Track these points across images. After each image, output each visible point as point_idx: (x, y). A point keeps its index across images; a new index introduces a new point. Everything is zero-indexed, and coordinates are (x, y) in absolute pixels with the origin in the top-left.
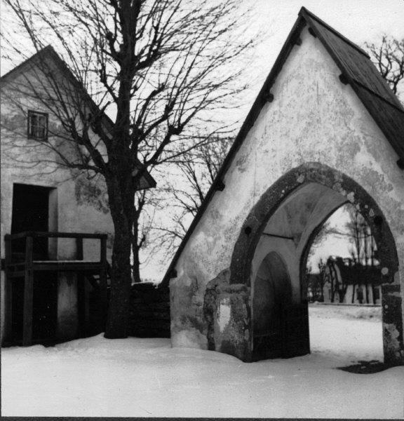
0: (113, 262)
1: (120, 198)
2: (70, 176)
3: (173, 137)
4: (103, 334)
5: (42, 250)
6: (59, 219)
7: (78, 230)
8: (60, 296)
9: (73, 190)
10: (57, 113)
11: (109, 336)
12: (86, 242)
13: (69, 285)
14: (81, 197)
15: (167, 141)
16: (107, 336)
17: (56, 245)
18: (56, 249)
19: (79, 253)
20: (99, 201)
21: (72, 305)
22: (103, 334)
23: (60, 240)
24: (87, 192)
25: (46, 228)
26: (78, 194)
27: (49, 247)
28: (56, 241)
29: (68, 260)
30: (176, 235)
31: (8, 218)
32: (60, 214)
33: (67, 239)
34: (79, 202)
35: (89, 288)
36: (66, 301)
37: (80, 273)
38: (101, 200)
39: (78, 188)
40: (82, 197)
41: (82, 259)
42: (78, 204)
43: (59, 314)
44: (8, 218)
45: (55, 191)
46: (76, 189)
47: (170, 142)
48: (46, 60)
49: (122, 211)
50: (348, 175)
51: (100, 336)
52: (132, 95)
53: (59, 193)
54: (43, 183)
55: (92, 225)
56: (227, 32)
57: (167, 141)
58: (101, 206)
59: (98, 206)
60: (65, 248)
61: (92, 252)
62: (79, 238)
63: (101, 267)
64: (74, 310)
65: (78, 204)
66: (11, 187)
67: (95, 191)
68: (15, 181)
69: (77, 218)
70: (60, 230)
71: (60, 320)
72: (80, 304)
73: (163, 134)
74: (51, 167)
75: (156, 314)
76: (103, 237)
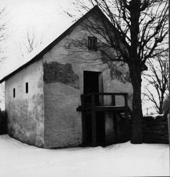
0: (133, 106)
1: (136, 74)
2: (108, 67)
3: (159, 44)
4: (130, 141)
5: (98, 102)
6: (104, 87)
7: (111, 92)
8: (106, 123)
9: (109, 73)
10: (104, 36)
11: (134, 142)
12: (117, 97)
13: (110, 118)
14: (113, 76)
15: (155, 45)
16: (132, 143)
17: (103, 99)
18: (103, 101)
19: (113, 103)
20: (121, 77)
21: (112, 127)
22: (130, 141)
23: (105, 96)
24: (116, 73)
25: (98, 91)
26: (112, 75)
27: (100, 100)
28: (103, 97)
29: (109, 106)
30: (146, 95)
31: (82, 87)
32: (104, 84)
33: (108, 96)
34: (112, 79)
35: (119, 119)
36: (109, 125)
37: (115, 112)
38: (122, 77)
39: (111, 72)
40: (114, 76)
41: (115, 105)
42: (112, 79)
43: (106, 131)
44: (82, 87)
45: (101, 74)
46: (111, 72)
47: (157, 46)
48: (95, 12)
49: (137, 81)
50: (77, 74)
51: (129, 143)
52: (140, 23)
53: (103, 74)
54: (97, 70)
55: (119, 89)
56: (69, 12)
57: (155, 45)
58: (122, 80)
59: (121, 80)
60: (107, 100)
61: (120, 102)
62: (113, 95)
63: (125, 109)
64: (112, 130)
65: (112, 79)
66: (83, 72)
67: (119, 73)
68: (84, 70)
69: (112, 86)
70: (104, 92)
71: (106, 134)
72: (115, 127)
73: (154, 43)
74: (99, 62)
75: (156, 132)
76: (125, 95)
